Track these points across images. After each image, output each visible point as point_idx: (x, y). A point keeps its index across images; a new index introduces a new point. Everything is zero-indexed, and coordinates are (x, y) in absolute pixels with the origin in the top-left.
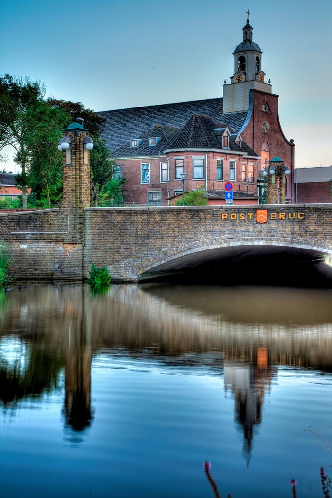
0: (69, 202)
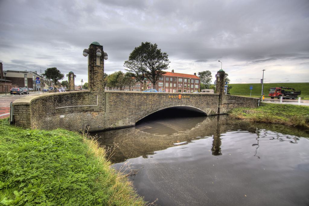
0: (98, 88)
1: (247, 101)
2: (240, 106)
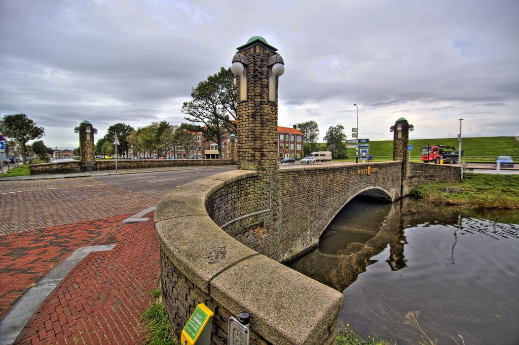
1: (441, 172)
2: (430, 179)
